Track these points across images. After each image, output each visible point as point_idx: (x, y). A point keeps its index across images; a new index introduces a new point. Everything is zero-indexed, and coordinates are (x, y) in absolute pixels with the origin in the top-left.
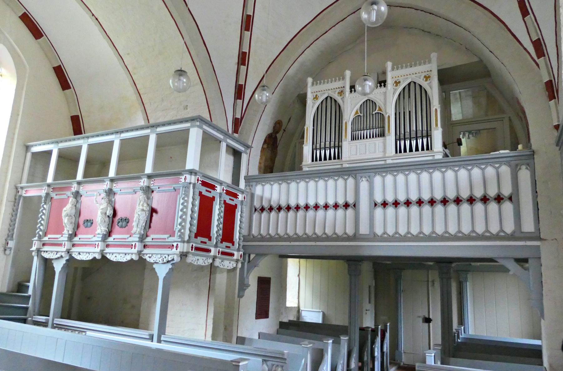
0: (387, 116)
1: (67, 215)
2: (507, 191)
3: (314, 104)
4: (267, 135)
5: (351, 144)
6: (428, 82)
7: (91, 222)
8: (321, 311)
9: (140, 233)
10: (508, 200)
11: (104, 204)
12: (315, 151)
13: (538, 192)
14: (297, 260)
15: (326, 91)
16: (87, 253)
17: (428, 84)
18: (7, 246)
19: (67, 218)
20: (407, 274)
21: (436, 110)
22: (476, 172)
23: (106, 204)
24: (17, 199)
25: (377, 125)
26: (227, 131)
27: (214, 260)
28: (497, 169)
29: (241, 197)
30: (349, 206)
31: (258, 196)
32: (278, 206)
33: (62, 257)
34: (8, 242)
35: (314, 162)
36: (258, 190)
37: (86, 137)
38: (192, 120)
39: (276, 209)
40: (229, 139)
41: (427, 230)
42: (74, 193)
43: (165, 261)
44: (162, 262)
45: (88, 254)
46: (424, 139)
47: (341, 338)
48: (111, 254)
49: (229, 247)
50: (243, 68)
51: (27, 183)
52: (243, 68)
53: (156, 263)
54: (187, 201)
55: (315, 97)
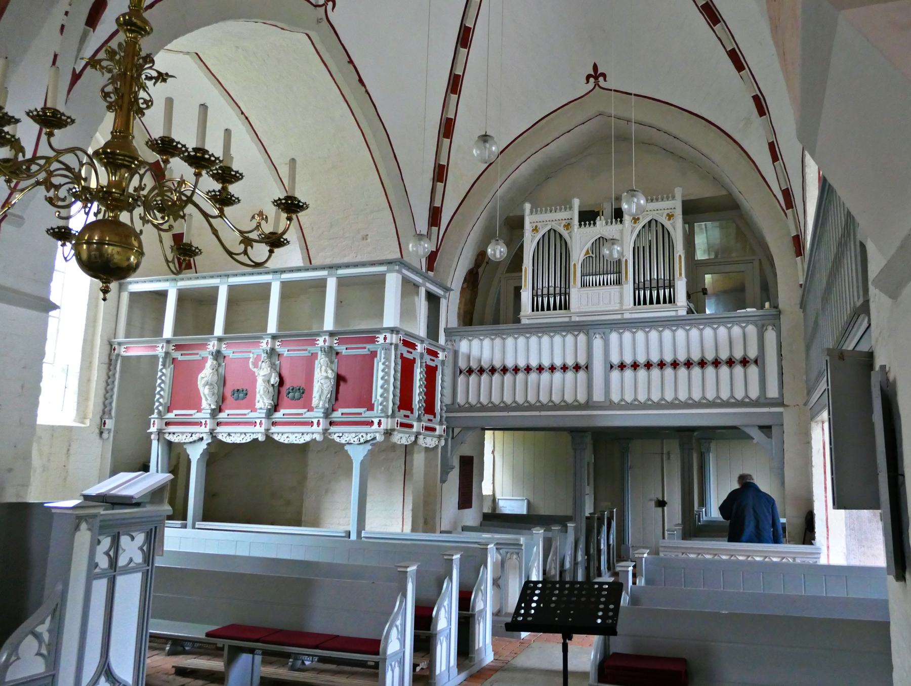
0: (624, 260)
1: (207, 384)
2: (753, 353)
3: (533, 237)
4: (468, 270)
5: (581, 292)
6: (671, 221)
7: (244, 392)
8: (525, 498)
9: (323, 407)
10: (754, 363)
11: (265, 369)
12: (536, 298)
13: (783, 355)
14: (502, 432)
15: (548, 222)
16: (241, 433)
17: (671, 224)
18: (104, 426)
19: (207, 387)
20: (636, 446)
21: (680, 256)
22: (722, 331)
23: (269, 369)
24: (111, 360)
25: (612, 270)
26: (420, 268)
27: (416, 437)
28: (743, 328)
29: (441, 355)
30: (580, 368)
31: (463, 354)
32: (491, 366)
33: (202, 439)
34: (105, 421)
35: (535, 312)
36: (464, 346)
37: (226, 276)
38: (389, 263)
39: (488, 371)
40: (428, 282)
41: (669, 397)
42: (214, 354)
43: (362, 441)
44: (358, 442)
45: (243, 436)
46: (666, 290)
47: (568, 525)
48: (280, 435)
49: (408, 416)
50: (440, 185)
51: (126, 337)
52: (440, 185)
53: (348, 443)
54: (388, 367)
55: (534, 228)
